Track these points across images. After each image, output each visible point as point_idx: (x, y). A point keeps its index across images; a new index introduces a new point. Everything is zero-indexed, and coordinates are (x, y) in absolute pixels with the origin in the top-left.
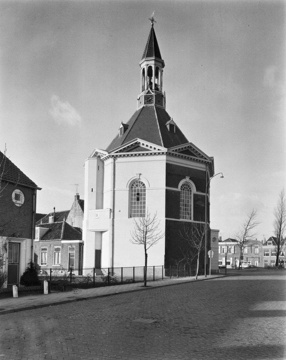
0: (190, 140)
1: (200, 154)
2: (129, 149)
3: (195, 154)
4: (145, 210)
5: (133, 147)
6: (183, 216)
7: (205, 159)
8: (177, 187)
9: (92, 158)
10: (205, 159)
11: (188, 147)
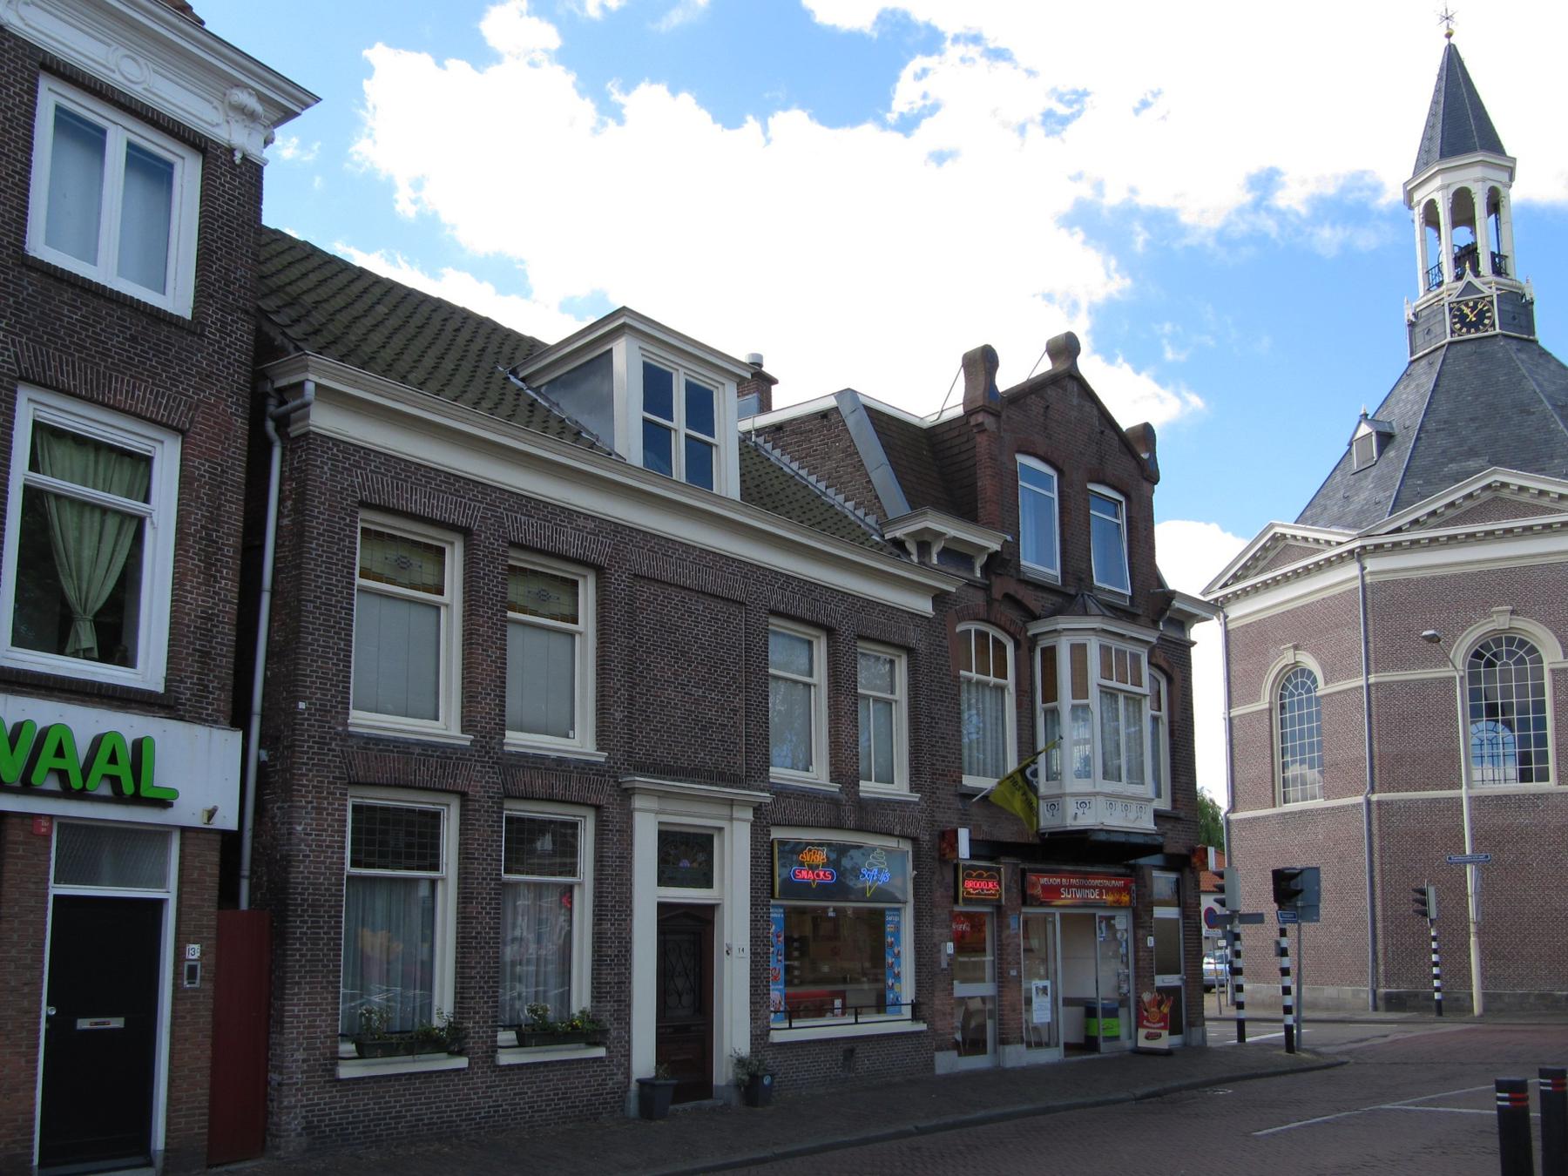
2: (1451, 513)
5: (1469, 504)
6: (339, 848)
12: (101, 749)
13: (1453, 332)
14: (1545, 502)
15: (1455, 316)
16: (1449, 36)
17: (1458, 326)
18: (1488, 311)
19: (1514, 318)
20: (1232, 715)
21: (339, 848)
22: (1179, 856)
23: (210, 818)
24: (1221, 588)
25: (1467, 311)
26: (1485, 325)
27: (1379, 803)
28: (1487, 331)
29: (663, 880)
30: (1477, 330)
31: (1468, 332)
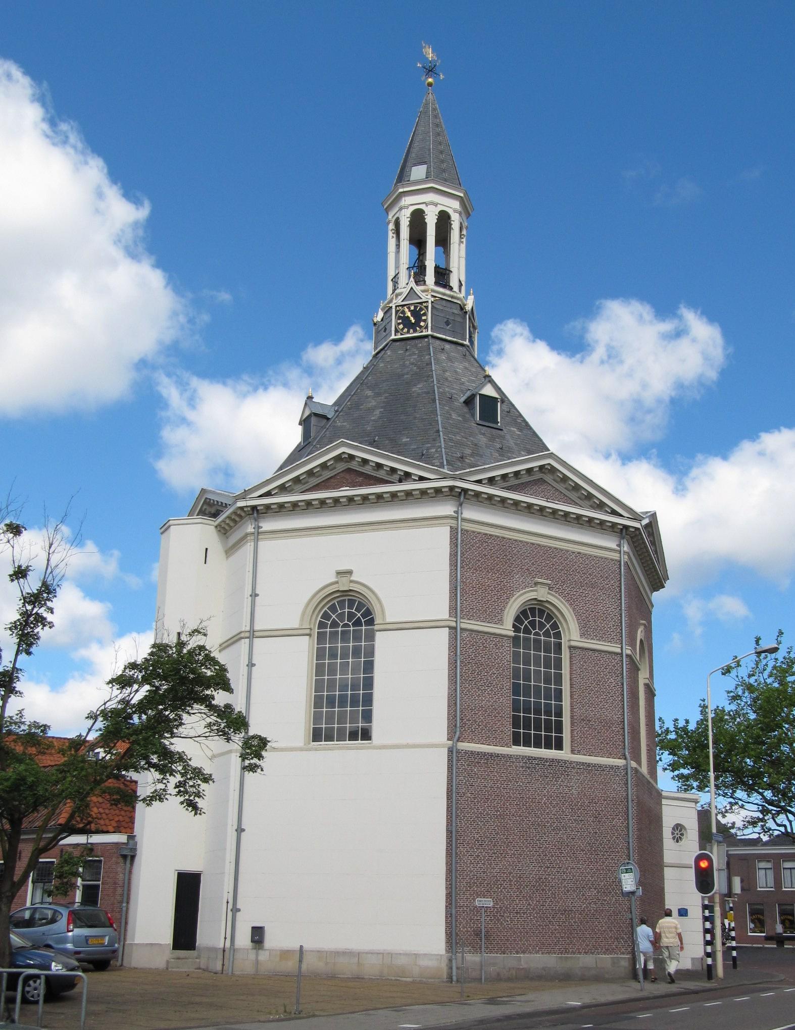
0: (552, 447)
1: (577, 488)
2: (314, 481)
4: (552, 749)
5: (327, 474)
6: (538, 738)
7: (614, 513)
8: (500, 621)
9: (231, 531)
10: (614, 513)
11: (541, 468)
12: (230, 940)
13: (396, 331)
14: (381, 474)
15: (399, 318)
17: (401, 326)
18: (425, 314)
21: (538, 738)
22: (33, 595)
23: (789, 653)
26: (421, 327)
28: (422, 332)
29: (316, 677)
30: (415, 331)
31: (408, 332)
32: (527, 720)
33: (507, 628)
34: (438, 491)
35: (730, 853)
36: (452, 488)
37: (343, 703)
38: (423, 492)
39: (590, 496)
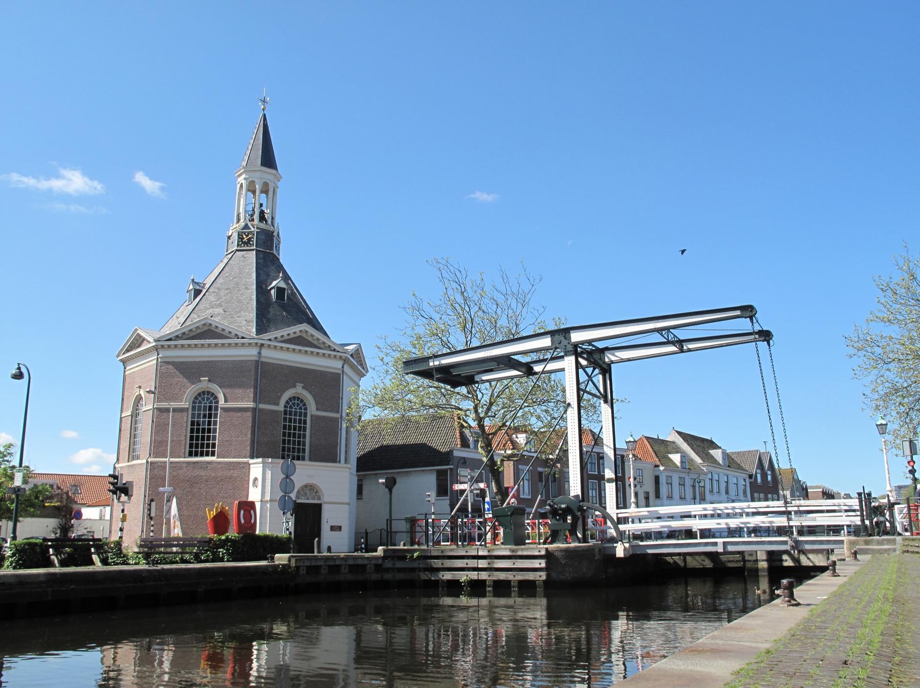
3: (316, 343)
16: (263, 110)
17: (240, 243)
18: (253, 238)
19: (264, 242)
20: (122, 416)
24: (124, 354)
25: (245, 236)
26: (250, 244)
27: (152, 463)
30: (247, 246)
31: (244, 246)
32: (289, 434)
33: (281, 408)
34: (250, 344)
35: (620, 516)
36: (256, 344)
37: (204, 430)
38: (243, 344)
39: (329, 347)
